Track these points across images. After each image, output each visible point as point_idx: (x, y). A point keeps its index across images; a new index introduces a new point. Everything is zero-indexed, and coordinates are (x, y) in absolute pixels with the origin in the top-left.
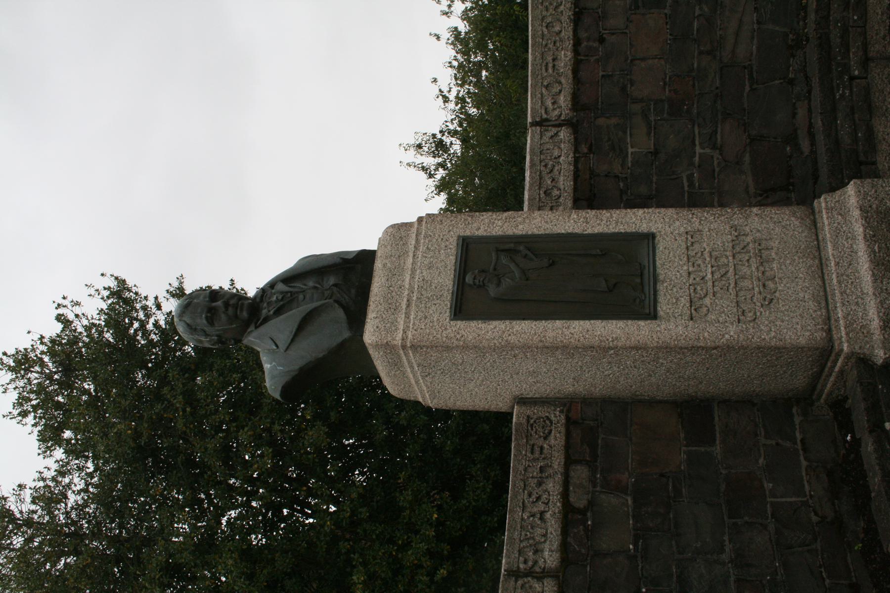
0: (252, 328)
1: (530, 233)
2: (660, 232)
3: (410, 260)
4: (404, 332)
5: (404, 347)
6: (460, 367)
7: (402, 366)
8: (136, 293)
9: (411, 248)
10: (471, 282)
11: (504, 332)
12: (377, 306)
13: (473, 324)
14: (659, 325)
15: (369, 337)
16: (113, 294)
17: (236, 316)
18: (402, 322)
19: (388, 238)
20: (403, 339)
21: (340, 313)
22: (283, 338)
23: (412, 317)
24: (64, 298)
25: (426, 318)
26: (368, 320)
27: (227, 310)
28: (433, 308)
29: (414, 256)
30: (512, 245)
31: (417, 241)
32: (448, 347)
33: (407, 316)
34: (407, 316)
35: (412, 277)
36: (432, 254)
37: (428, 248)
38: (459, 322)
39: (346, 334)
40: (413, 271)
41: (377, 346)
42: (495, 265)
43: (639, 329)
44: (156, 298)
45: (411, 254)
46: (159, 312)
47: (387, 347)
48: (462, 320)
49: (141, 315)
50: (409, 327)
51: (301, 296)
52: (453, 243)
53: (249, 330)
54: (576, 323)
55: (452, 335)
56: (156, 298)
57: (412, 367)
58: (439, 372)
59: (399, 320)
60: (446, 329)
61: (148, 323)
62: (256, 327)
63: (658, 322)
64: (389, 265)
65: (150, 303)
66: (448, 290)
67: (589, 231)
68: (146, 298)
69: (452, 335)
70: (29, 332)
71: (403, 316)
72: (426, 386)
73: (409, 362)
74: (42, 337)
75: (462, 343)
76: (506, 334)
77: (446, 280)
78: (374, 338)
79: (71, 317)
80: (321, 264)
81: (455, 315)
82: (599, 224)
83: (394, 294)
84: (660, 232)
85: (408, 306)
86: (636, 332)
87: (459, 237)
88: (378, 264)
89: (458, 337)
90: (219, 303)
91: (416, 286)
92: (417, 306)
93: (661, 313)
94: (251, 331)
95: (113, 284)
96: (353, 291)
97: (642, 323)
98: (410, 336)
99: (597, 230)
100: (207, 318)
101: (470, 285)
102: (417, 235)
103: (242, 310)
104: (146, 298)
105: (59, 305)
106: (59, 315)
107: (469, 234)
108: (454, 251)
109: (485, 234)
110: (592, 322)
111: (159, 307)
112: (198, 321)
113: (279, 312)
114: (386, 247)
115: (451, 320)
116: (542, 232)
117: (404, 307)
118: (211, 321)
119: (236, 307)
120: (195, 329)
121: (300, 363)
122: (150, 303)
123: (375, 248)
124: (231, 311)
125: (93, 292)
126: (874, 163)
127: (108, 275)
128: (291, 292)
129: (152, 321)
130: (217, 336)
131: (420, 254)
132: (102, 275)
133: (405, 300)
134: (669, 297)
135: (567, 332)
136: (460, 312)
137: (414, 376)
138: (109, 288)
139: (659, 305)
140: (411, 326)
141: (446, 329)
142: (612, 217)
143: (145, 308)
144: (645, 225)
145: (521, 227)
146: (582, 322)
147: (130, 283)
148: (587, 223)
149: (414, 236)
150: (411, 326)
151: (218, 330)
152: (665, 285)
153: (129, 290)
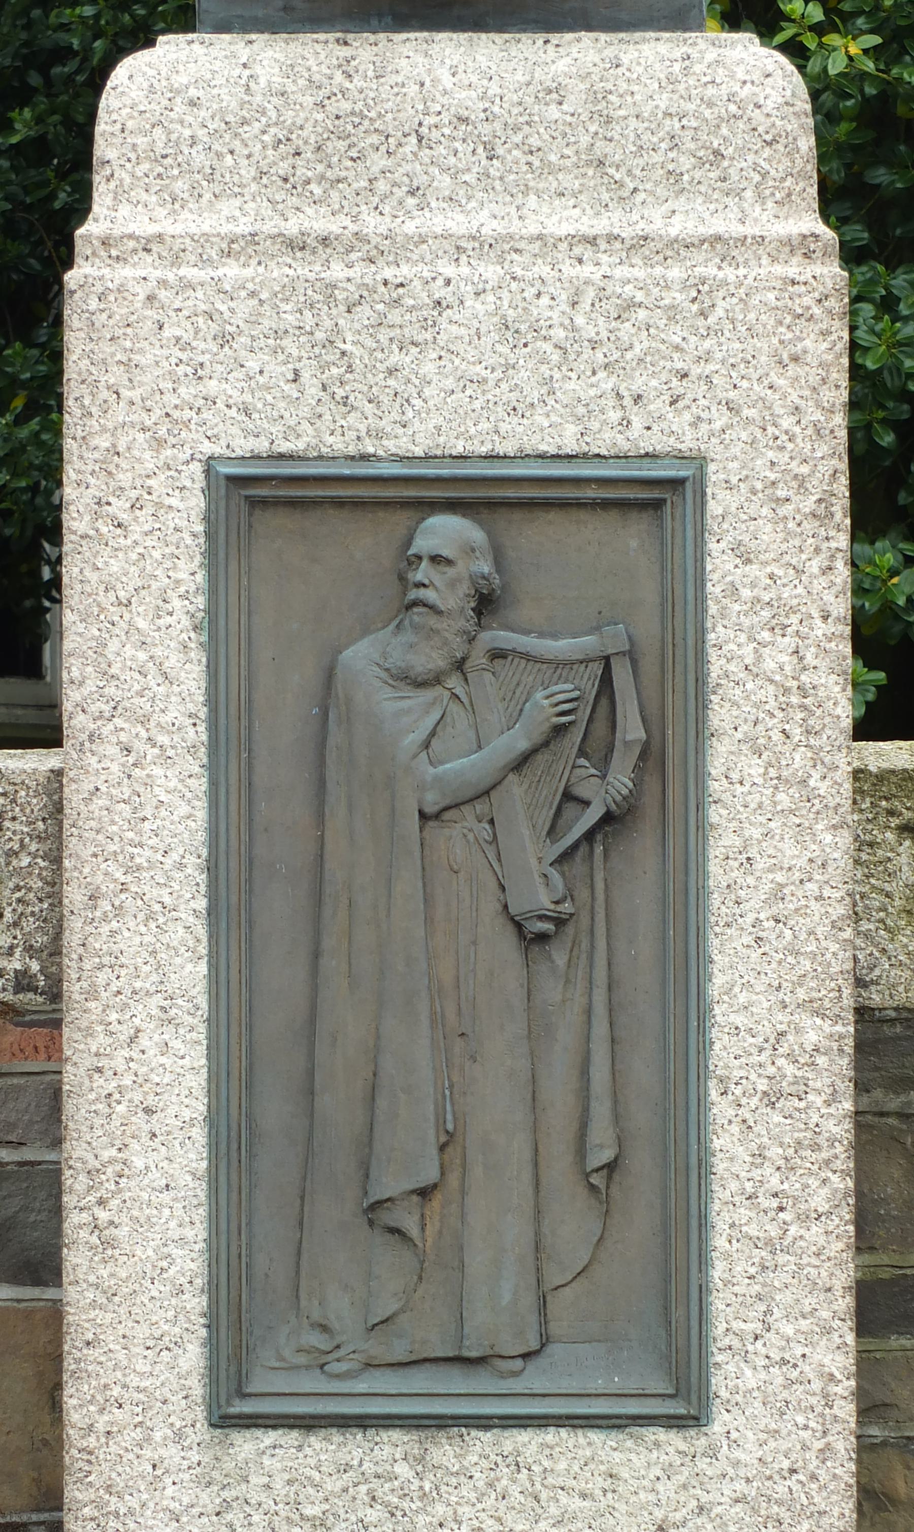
1: (715, 814)
2: (712, 1453)
10: (422, 544)
11: (144, 720)
13: (190, 572)
14: (179, 1436)
23: (231, 271)
25: (224, 340)
28: (278, 370)
30: (632, 730)
37: (632, 305)
38: (197, 502)
42: (527, 657)
43: (158, 1345)
50: (176, 260)
52: (654, 431)
54: (198, 1058)
55: (125, 479)
59: (228, 206)
63: (202, 1431)
66: (378, 435)
67: (721, 1108)
69: (125, 479)
76: (132, 732)
81: (233, 480)
82: (760, 1155)
83: (378, 161)
84: (712, 1453)
86: (142, 1332)
87: (700, 461)
89: (119, 507)
92: (289, 288)
93: (246, 1444)
97: (192, 1357)
98: (125, 272)
99: (729, 1149)
107: (714, 508)
108: (605, 441)
109: (713, 589)
110: (199, 1134)
116: (718, 873)
126: (60, 1073)
134: (333, 1485)
135: (143, 1013)
136: (255, 503)
139: (293, 1437)
141: (160, 443)
142: (803, 1218)
144: (750, 1379)
145: (754, 768)
146: (198, 1082)
148: (771, 1099)
149: (724, 224)
152: (403, 1470)
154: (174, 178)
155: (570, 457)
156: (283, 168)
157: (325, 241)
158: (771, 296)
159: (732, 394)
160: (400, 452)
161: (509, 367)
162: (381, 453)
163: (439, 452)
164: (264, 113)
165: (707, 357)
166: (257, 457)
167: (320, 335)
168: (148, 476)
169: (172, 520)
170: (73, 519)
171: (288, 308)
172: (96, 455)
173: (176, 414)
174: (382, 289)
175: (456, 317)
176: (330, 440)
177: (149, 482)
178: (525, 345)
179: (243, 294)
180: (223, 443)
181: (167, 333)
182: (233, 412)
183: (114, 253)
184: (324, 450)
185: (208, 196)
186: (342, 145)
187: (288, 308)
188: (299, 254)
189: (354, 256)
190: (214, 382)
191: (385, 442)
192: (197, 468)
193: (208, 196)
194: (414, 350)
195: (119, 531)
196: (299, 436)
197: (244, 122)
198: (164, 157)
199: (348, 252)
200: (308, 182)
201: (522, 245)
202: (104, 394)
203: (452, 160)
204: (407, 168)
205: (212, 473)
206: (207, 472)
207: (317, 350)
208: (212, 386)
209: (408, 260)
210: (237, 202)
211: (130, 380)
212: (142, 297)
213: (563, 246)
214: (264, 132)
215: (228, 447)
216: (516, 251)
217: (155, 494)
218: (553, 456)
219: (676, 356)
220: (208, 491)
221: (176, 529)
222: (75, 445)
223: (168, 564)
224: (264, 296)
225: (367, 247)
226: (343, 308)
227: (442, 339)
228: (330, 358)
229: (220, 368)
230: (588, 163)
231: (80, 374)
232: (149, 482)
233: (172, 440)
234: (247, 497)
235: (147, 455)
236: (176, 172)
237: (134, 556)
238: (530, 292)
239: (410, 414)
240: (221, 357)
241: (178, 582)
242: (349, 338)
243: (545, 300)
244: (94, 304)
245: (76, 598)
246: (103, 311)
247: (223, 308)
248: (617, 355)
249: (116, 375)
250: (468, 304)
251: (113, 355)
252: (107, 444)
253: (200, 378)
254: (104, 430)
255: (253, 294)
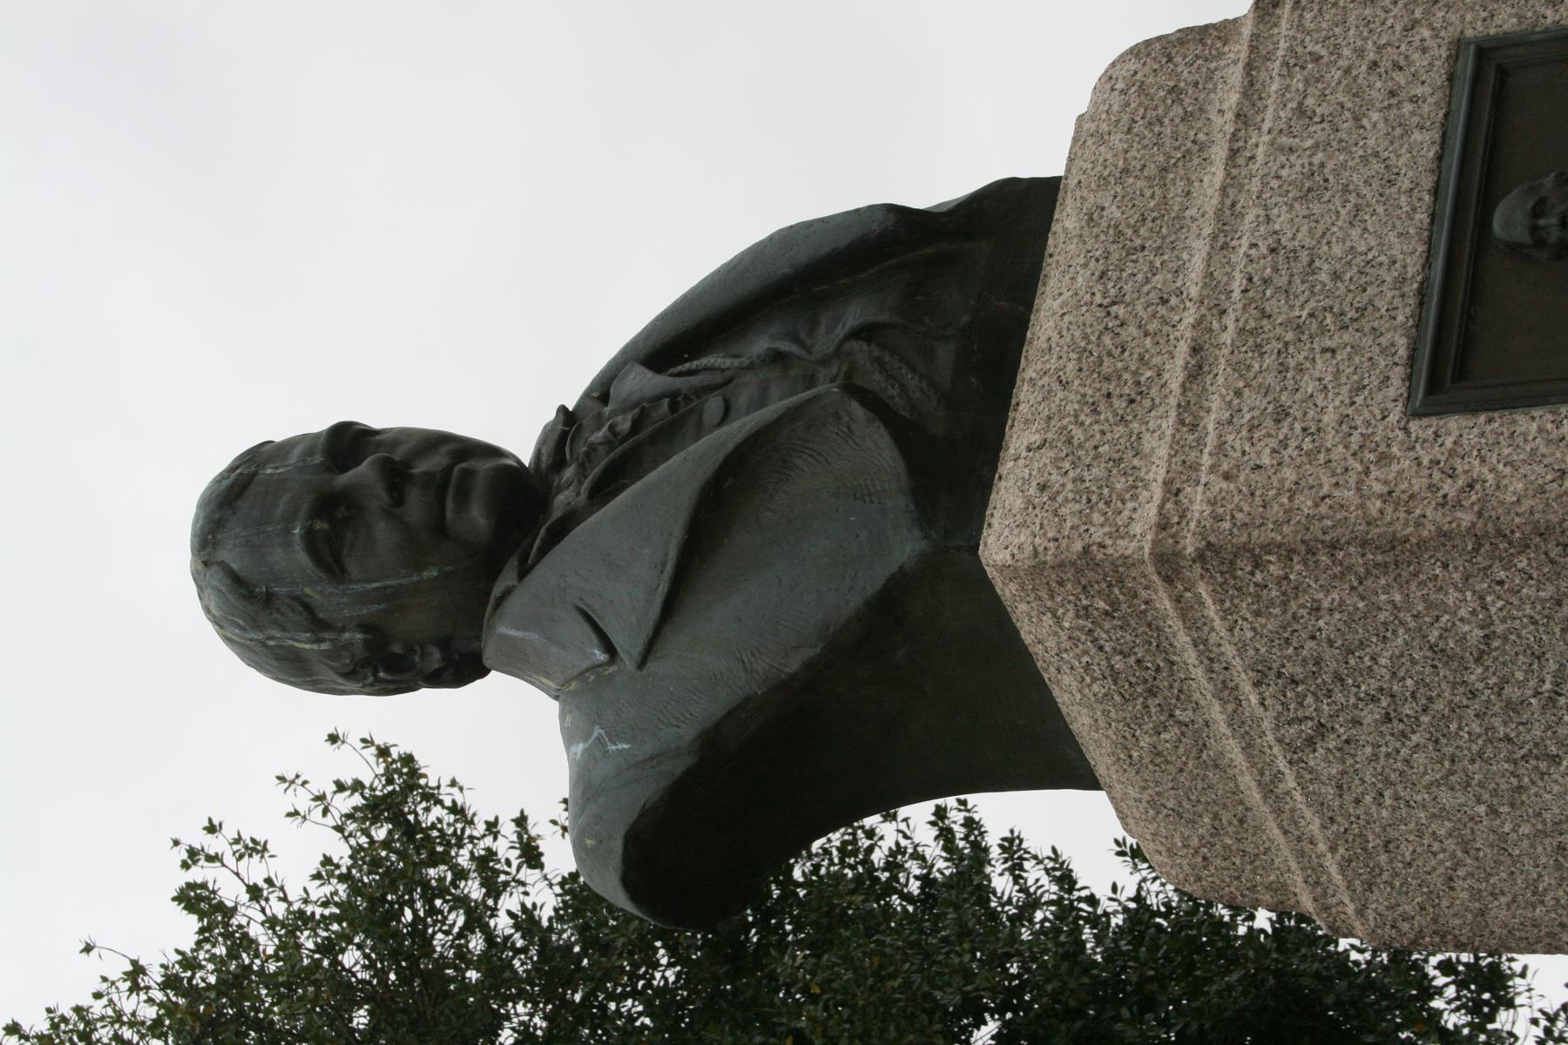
0: (507, 578)
3: (1216, 174)
4: (1172, 491)
5: (1168, 563)
6: (1474, 676)
7: (1184, 697)
8: (456, 809)
9: (1223, 123)
10: (1520, 234)
12: (1048, 395)
13: (1529, 423)
15: (1004, 541)
16: (375, 809)
17: (440, 528)
18: (1163, 452)
19: (1116, 100)
20: (1163, 526)
21: (877, 452)
22: (629, 603)
24: (212, 829)
25: (1281, 414)
26: (1006, 467)
27: (399, 501)
28: (1321, 366)
29: (1233, 153)
31: (1252, 89)
32: (1393, 543)
33: (1189, 419)
34: (1189, 419)
35: (1221, 244)
36: (1320, 132)
37: (1301, 110)
38: (1454, 423)
39: (906, 547)
40: (1228, 216)
41: (1037, 572)
44: (521, 821)
45: (1219, 152)
46: (528, 874)
47: (1089, 576)
48: (1471, 408)
49: (474, 889)
50: (1195, 467)
51: (714, 405)
53: (497, 591)
55: (1418, 484)
56: (521, 821)
57: (1227, 692)
58: (1370, 715)
59: (1149, 442)
60: (1384, 459)
61: (494, 911)
62: (523, 573)
64: (1113, 212)
65: (505, 848)
66: (1401, 281)
68: (492, 827)
69: (1418, 484)
70: (88, 949)
71: (1168, 425)
72: (1320, 806)
73: (1211, 661)
74: (136, 972)
75: (1466, 518)
77: (1392, 240)
78: (1024, 537)
79: (230, 891)
80: (803, 255)
81: (1433, 386)
85: (1195, 373)
88: (1067, 220)
89: (1449, 488)
90: (364, 471)
91: (1237, 285)
92: (1238, 367)
94: (507, 593)
95: (368, 771)
96: (945, 354)
100: (310, 538)
101: (1514, 248)
102: (1249, 67)
103: (463, 496)
104: (492, 827)
105: (193, 853)
106: (191, 886)
108: (1432, 109)
111: (531, 855)
112: (277, 556)
113: (603, 491)
114: (1101, 138)
115: (1415, 413)
117: (1175, 377)
118: (329, 555)
119: (439, 485)
120: (269, 598)
121: (704, 711)
122: (505, 848)
123: (1059, 171)
124: (416, 505)
125: (303, 801)
127: (354, 740)
128: (673, 396)
129: (510, 902)
130: (365, 627)
131: (1260, 143)
132: (333, 739)
133: (1183, 349)
136: (1461, 374)
137: (1248, 748)
138: (357, 786)
140: (1206, 460)
143: (485, 862)
147: (434, 772)
149: (1236, 75)
150: (1206, 460)
151: (363, 598)
153: (431, 797)
154: (1112, 489)
155: (1444, 135)
156: (1120, 404)
157: (1195, 350)
158: (1308, 16)
159: (1398, 28)
160: (1421, 261)
161: (1346, 190)
162: (1419, 278)
163: (1426, 233)
164: (1064, 428)
165: (1360, 53)
166: (1410, 378)
167: (1290, 336)
168: (1419, 464)
169: (1472, 437)
170: (1459, 525)
171: (1257, 366)
172: (1389, 510)
173: (1354, 447)
174: (1251, 293)
175: (1290, 235)
176: (1401, 318)
177: (1426, 462)
178: (1326, 180)
179: (1236, 402)
180: (1390, 405)
181: (1266, 460)
182: (1359, 400)
183: (1176, 520)
184: (1411, 323)
185: (1136, 462)
186: (1107, 362)
187: (1257, 366)
188: (1206, 369)
189: (1215, 325)
190: (1326, 418)
191: (1409, 275)
192: (1414, 426)
193: (1136, 462)
194: (1318, 263)
195: (1478, 487)
196: (1393, 344)
197: (1069, 441)
198: (1089, 501)
199: (1211, 330)
200: (1138, 383)
201: (1228, 202)
202: (1323, 509)
203: (1140, 277)
204: (1139, 308)
205: (1422, 410)
206: (1418, 415)
207: (1304, 338)
208: (1329, 418)
209: (1227, 284)
210: (1146, 436)
211: (1311, 488)
212: (1224, 485)
213: (1235, 172)
214: (1082, 424)
215: (1395, 401)
216: (1233, 205)
217: (1439, 457)
218: (1442, 148)
219: (1354, 73)
220: (1441, 411)
221: (1483, 434)
222: (1376, 530)
223: (1520, 440)
224: (1241, 384)
225: (1209, 318)
226: (1265, 322)
227: (1308, 242)
228: (1314, 326)
229: (1311, 413)
230: (1163, 178)
231: (1297, 532)
232: (1426, 462)
233: (1383, 448)
234: (1453, 382)
235: (1395, 467)
236: (1106, 491)
237: (1508, 470)
238: (1275, 183)
239: (1383, 258)
240: (1299, 414)
241: (1541, 430)
242: (1297, 313)
243: (1284, 173)
244: (1227, 525)
245: (1550, 517)
246: (1233, 517)
247: (1248, 416)
248: (1348, 115)
249: (1305, 503)
250: (1277, 227)
251: (1282, 505)
252: (1378, 503)
253: (1319, 430)
254: (1362, 506)
255: (1238, 393)
